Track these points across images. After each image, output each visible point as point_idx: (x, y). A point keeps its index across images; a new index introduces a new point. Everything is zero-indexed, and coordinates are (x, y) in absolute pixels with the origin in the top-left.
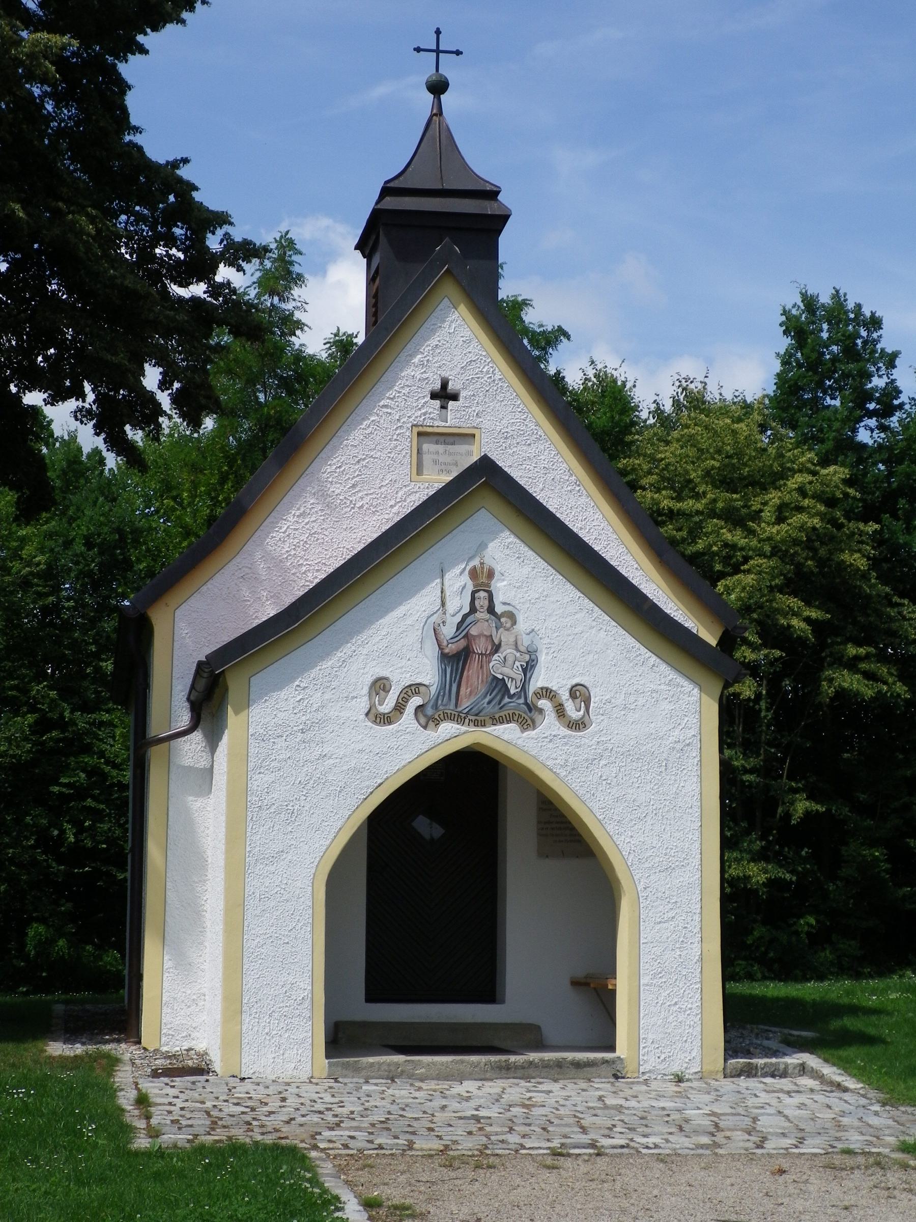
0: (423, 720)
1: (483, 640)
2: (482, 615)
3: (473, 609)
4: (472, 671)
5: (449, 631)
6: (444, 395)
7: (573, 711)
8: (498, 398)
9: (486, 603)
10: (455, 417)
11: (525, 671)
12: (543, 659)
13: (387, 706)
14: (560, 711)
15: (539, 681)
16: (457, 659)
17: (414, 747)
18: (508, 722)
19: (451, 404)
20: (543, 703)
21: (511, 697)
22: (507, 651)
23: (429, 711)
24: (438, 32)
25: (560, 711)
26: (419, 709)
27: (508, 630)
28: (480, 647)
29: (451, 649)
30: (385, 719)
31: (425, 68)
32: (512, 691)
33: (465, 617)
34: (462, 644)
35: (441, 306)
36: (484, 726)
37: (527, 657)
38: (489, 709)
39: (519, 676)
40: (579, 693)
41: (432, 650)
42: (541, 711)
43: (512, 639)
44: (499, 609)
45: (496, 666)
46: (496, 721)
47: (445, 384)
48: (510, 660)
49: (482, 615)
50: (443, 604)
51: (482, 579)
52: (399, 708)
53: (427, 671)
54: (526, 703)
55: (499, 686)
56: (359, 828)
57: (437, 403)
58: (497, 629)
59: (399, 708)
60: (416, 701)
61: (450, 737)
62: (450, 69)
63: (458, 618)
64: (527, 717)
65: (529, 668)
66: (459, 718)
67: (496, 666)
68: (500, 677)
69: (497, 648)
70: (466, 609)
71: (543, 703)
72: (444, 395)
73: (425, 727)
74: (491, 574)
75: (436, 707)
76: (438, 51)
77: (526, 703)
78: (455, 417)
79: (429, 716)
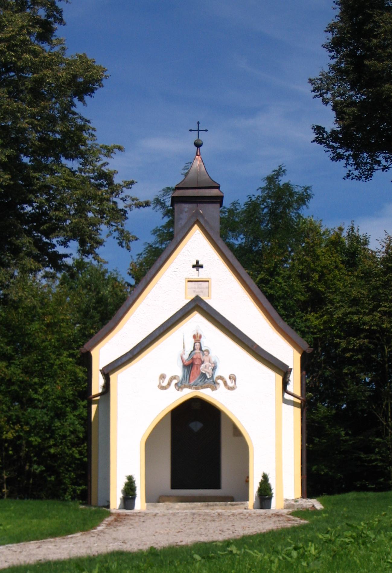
0: (177, 388)
1: (198, 360)
2: (197, 351)
3: (194, 349)
4: (194, 370)
5: (186, 357)
6: (198, 266)
7: (230, 383)
8: (373, 283)
9: (199, 347)
10: (202, 274)
11: (213, 370)
12: (219, 365)
13: (165, 384)
14: (225, 384)
15: (217, 373)
16: (190, 366)
17: (176, 397)
18: (207, 388)
19: (200, 269)
20: (219, 381)
21: (208, 379)
22: (206, 363)
23: (180, 385)
24: (198, 123)
25: (225, 384)
26: (176, 384)
27: (207, 356)
28: (197, 362)
29: (187, 363)
30: (163, 388)
31: (194, 136)
32: (208, 377)
33: (192, 352)
34: (191, 361)
35: (196, 233)
36: (198, 389)
37: (213, 365)
38: (201, 384)
39: (211, 371)
40: (233, 378)
41: (181, 364)
42: (218, 384)
43: (208, 359)
44: (203, 349)
45: (202, 368)
46: (203, 387)
47: (197, 262)
48: (207, 366)
49: (197, 351)
50: (184, 348)
51: (197, 338)
52: (169, 384)
53: (179, 372)
54: (213, 381)
55: (204, 376)
56: (168, 413)
57: (195, 269)
58: (203, 355)
59: (169, 384)
60: (175, 381)
61: (187, 394)
62: (203, 137)
63: (189, 352)
64: (214, 385)
65: (214, 369)
66: (190, 387)
67: (202, 368)
68: (204, 372)
69: (203, 362)
70: (192, 349)
71: (219, 381)
72: (198, 266)
73: (178, 390)
74: (200, 337)
75: (182, 383)
76: (198, 130)
77: (213, 381)
78: (202, 274)
79: (179, 387)
